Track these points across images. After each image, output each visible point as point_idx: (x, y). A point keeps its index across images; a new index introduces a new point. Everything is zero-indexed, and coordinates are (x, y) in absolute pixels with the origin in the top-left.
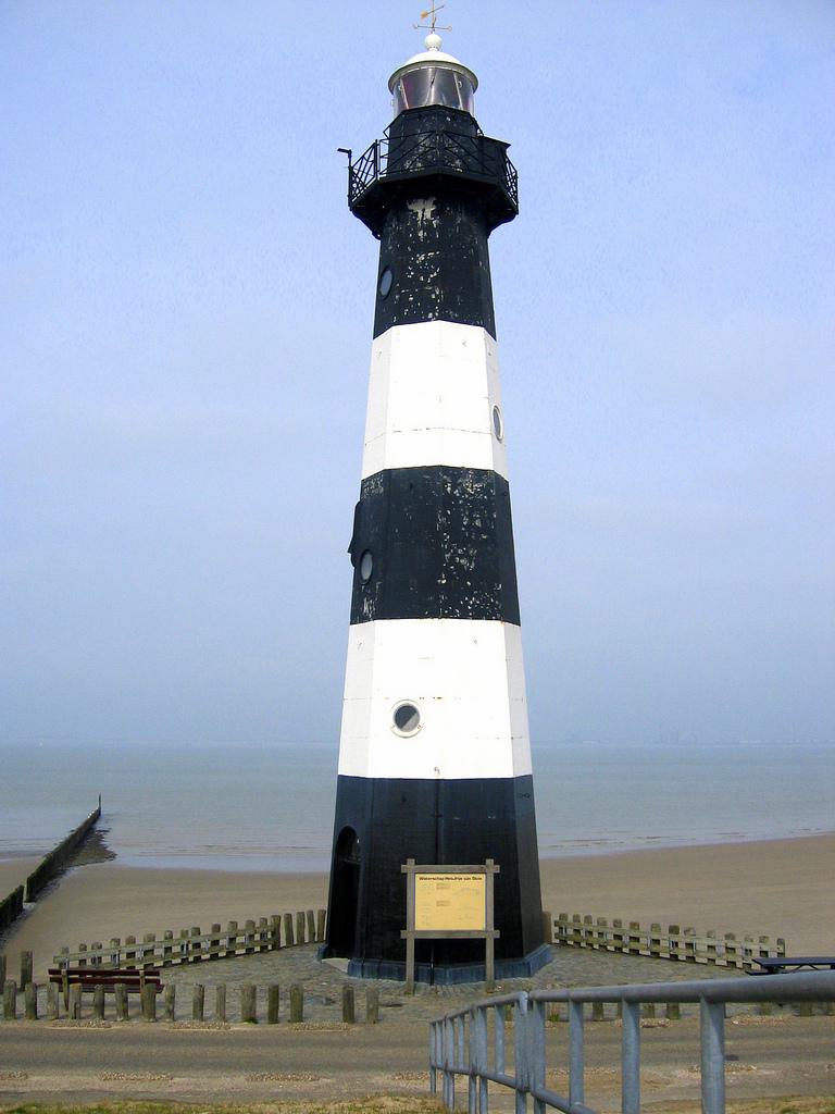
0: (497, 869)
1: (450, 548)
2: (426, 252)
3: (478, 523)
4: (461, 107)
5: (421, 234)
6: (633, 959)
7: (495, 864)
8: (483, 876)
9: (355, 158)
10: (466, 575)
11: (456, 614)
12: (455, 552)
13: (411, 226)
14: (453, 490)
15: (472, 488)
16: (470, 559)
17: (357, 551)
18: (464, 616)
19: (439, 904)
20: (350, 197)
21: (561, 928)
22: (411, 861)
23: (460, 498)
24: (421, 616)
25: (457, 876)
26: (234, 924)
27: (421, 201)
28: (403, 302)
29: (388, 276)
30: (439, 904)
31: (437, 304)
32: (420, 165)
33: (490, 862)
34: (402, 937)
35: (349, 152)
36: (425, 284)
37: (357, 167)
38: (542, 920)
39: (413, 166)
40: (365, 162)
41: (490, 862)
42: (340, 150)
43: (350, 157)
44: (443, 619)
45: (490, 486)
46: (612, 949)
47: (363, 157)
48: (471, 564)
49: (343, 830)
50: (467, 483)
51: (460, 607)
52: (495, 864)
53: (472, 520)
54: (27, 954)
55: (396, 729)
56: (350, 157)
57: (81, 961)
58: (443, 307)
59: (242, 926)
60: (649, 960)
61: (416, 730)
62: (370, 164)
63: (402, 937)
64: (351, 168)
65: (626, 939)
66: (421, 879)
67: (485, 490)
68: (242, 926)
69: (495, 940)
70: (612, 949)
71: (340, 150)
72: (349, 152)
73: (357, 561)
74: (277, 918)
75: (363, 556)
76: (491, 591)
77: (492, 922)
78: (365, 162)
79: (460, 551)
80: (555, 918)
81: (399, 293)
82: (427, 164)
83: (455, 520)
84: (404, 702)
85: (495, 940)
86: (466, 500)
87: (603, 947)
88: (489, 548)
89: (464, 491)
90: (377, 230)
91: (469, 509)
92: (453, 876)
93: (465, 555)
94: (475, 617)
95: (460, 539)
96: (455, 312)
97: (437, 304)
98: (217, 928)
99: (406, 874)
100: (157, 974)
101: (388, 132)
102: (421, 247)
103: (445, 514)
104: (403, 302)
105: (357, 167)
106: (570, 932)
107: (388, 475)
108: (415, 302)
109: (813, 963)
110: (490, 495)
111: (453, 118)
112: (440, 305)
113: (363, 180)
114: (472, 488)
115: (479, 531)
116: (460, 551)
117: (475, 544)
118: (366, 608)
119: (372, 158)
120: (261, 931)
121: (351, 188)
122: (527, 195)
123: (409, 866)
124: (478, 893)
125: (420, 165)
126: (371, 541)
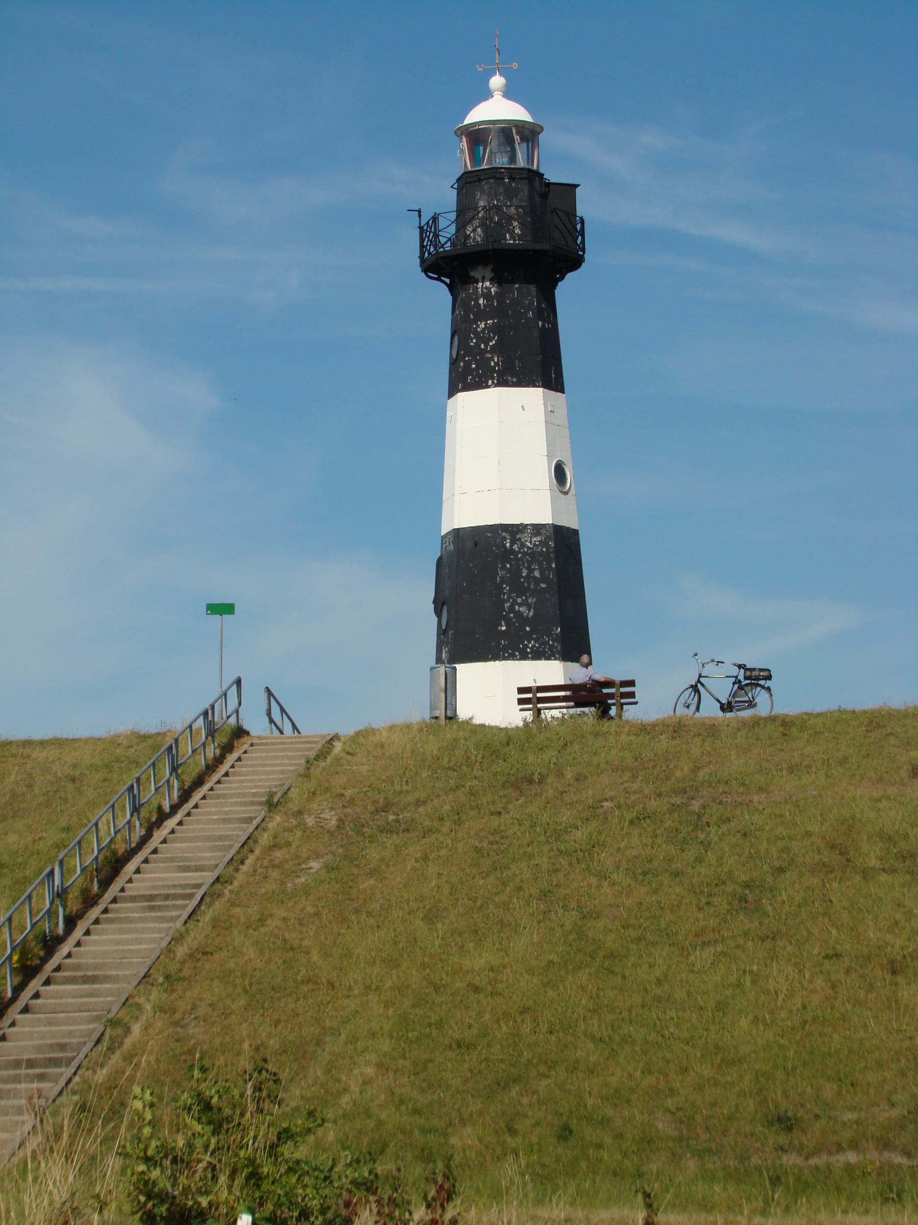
1: (509, 597)
3: (537, 574)
5: (481, 301)
12: (515, 602)
14: (512, 544)
15: (531, 542)
16: (529, 608)
17: (439, 604)
18: (524, 657)
24: (484, 658)
27: (480, 268)
28: (467, 369)
29: (456, 338)
31: (495, 371)
36: (485, 351)
39: (476, 235)
43: (420, 216)
44: (504, 662)
48: (529, 611)
51: (520, 650)
53: (531, 571)
56: (420, 216)
58: (501, 374)
64: (421, 228)
72: (419, 211)
73: (438, 612)
81: (464, 361)
83: (516, 573)
86: (525, 554)
89: (523, 545)
93: (525, 603)
94: (533, 659)
95: (519, 590)
96: (512, 377)
97: (495, 371)
102: (482, 315)
103: (504, 567)
104: (467, 369)
107: (457, 533)
109: (175, 886)
111: (512, 179)
112: (498, 372)
115: (537, 581)
116: (519, 600)
121: (422, 246)
122: (589, 256)
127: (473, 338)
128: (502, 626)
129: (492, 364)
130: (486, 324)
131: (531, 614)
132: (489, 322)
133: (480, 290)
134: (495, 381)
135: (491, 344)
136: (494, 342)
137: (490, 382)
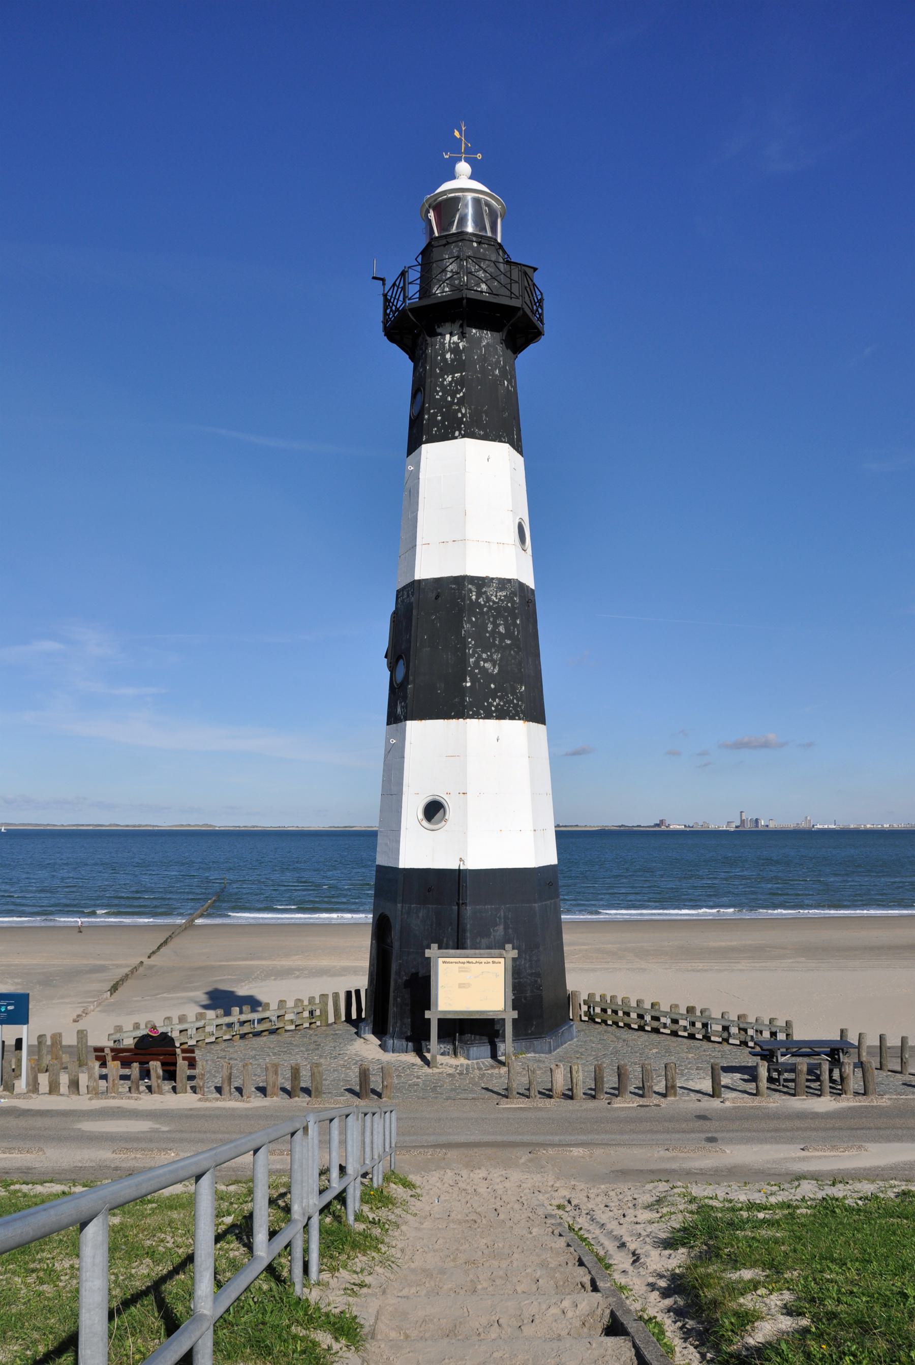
0: (514, 954)
1: (474, 652)
2: (453, 374)
3: (502, 629)
4: (489, 234)
5: (448, 356)
6: (654, 1036)
7: (513, 948)
8: (502, 960)
9: (389, 284)
10: (489, 677)
11: (481, 714)
12: (480, 657)
13: (440, 349)
14: (478, 598)
15: (496, 596)
18: (488, 716)
19: (461, 986)
20: (385, 323)
21: (589, 1007)
22: (435, 946)
23: (485, 606)
25: (478, 960)
26: (282, 1003)
30: (461, 986)
32: (447, 289)
33: (509, 946)
34: (426, 1016)
35: (383, 280)
37: (390, 294)
38: (566, 1000)
39: (441, 291)
40: (396, 288)
41: (428, 953)
42: (374, 278)
43: (384, 284)
45: (514, 594)
46: (636, 1027)
47: (394, 285)
48: (494, 667)
49: (380, 916)
50: (490, 591)
51: (483, 708)
52: (513, 948)
53: (496, 626)
54: (336, 993)
55: (425, 823)
56: (384, 284)
57: (115, 1042)
58: (468, 426)
59: (290, 1004)
60: (669, 1037)
61: (443, 823)
62: (400, 290)
63: (426, 1016)
64: (385, 296)
65: (648, 1018)
66: (444, 962)
67: (509, 598)
68: (290, 1004)
69: (514, 1020)
70: (636, 1027)
71: (374, 278)
73: (392, 667)
74: (324, 997)
75: (397, 661)
76: (514, 693)
77: (510, 1003)
78: (396, 288)
79: (484, 656)
80: (584, 996)
81: (429, 413)
82: (454, 288)
84: (434, 797)
85: (514, 1020)
86: (490, 608)
87: (615, 1023)
88: (512, 652)
89: (488, 599)
90: (412, 361)
91: (493, 616)
92: (474, 960)
97: (463, 423)
98: (282, 1003)
99: (429, 958)
100: (193, 1052)
101: (420, 259)
103: (470, 621)
105: (390, 294)
106: (598, 1010)
108: (442, 421)
110: (513, 602)
111: (479, 243)
113: (395, 304)
114: (496, 596)
115: (503, 637)
116: (484, 656)
117: (500, 648)
118: (399, 710)
119: (401, 285)
120: (309, 1008)
121: (385, 314)
123: (432, 952)
124: (497, 976)
125: (447, 289)
126: (403, 647)
127: (439, 391)
128: (466, 682)
129: (460, 415)
130: (453, 378)
131: (496, 671)
132: (456, 375)
133: (447, 345)
134: (463, 432)
135: (458, 396)
136: (461, 394)
137: (457, 433)
